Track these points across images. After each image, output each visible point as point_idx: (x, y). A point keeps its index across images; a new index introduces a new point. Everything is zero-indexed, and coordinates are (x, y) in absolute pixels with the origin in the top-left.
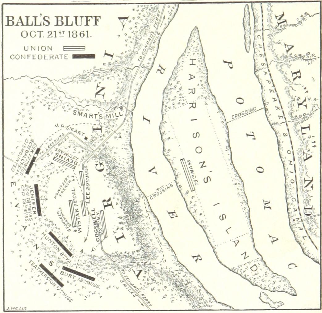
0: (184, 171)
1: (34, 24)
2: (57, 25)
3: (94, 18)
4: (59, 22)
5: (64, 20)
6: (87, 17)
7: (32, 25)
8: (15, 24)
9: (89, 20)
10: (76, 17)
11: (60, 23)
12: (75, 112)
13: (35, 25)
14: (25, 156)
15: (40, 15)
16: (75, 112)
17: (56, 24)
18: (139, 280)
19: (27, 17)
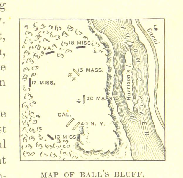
0: (77, 127)
1: (97, 176)
2: (81, 177)
3: (137, 173)
4: (82, 175)
5: (120, 174)
6: (133, 172)
7: (96, 176)
8: (86, 176)
9: (134, 174)
10: (127, 172)
11: (117, 175)
12: (48, 83)
13: (99, 176)
14: (66, 115)
15: (103, 171)
16: (48, 83)
17: (81, 176)
18: (25, 156)
19: (93, 173)
